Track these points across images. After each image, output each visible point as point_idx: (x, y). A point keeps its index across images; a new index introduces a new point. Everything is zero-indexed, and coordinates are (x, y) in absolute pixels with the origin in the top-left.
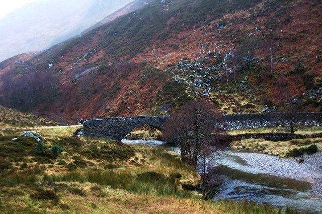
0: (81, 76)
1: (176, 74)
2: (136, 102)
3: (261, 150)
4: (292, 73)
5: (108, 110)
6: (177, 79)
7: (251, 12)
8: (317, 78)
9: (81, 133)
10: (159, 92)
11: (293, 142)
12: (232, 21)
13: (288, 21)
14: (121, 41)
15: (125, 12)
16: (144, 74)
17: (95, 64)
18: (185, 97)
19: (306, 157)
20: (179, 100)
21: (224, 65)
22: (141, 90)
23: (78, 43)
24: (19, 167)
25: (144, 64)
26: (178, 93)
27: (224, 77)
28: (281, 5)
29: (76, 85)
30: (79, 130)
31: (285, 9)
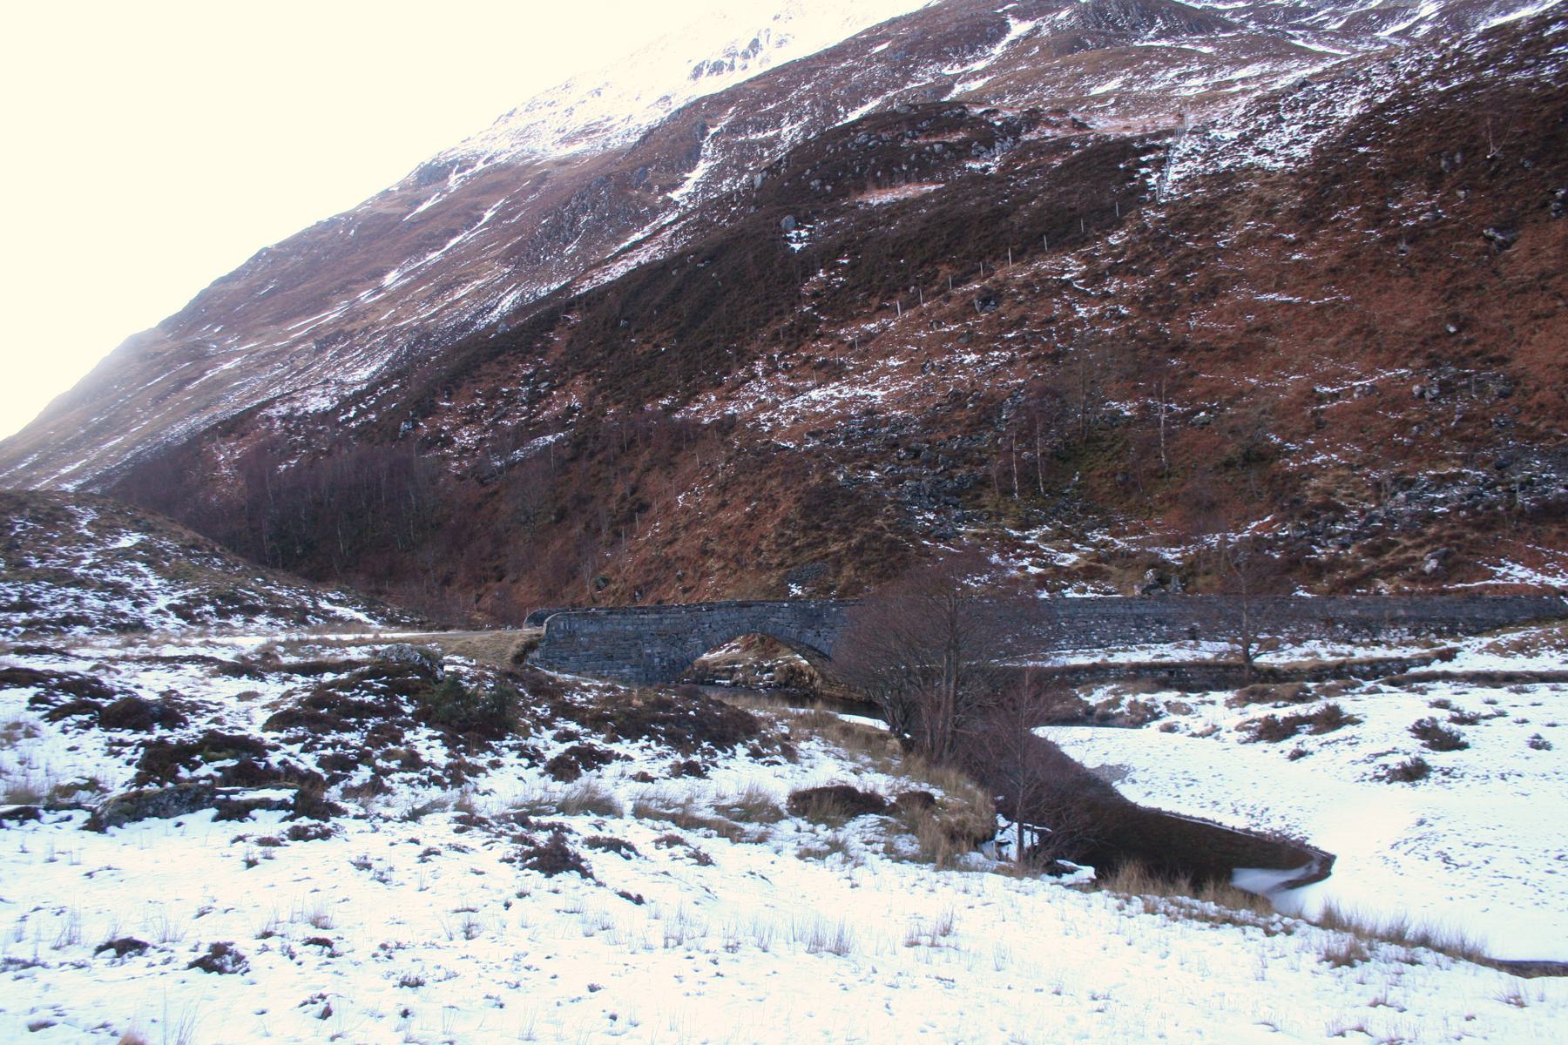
0: (511, 466)
1: (843, 461)
2: (705, 553)
3: (1141, 717)
4: (1229, 464)
5: (607, 581)
6: (847, 477)
7: (1089, 259)
8: (1314, 482)
9: (536, 655)
10: (785, 522)
11: (1252, 693)
12: (1027, 284)
13: (1213, 289)
14: (648, 347)
15: (234, 276)
16: (729, 460)
17: (559, 423)
18: (875, 538)
19: (1305, 739)
20: (860, 549)
21: (1003, 434)
22: (721, 515)
23: (497, 354)
24: (394, 765)
25: (728, 426)
26: (1472, 535)
27: (1006, 474)
28: (1188, 238)
29: (496, 493)
30: (530, 646)
31: (1199, 253)
